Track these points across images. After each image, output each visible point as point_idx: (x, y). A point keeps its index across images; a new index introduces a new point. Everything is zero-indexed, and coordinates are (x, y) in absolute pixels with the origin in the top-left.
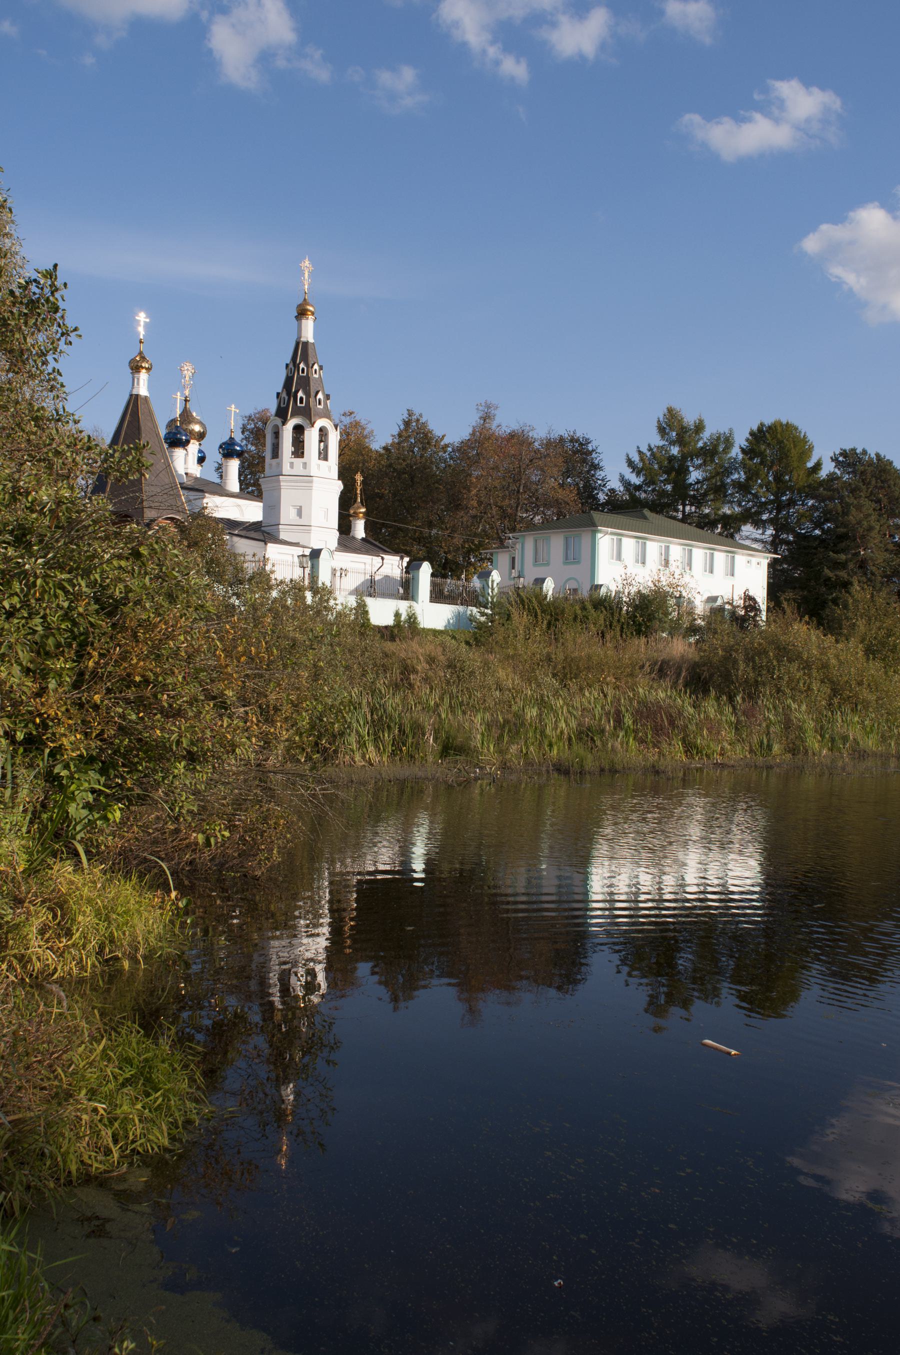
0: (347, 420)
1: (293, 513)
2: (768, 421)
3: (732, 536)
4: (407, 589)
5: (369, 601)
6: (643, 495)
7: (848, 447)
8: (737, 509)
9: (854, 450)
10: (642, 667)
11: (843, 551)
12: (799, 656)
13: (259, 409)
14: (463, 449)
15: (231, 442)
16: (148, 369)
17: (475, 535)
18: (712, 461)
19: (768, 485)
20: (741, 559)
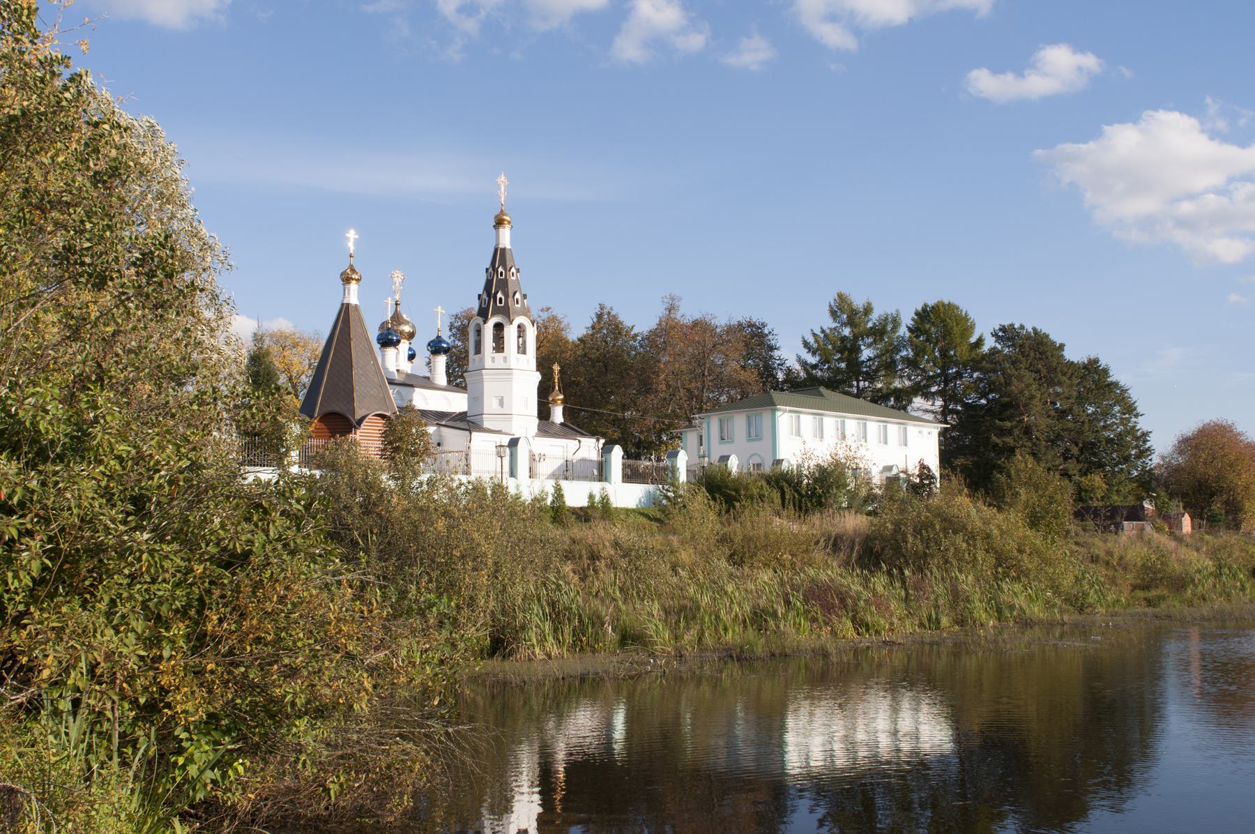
0: (545, 315)
1: (495, 403)
2: (931, 302)
3: (904, 408)
4: (602, 473)
5: (564, 484)
6: (820, 373)
7: (1006, 323)
8: (907, 383)
9: (1012, 325)
10: (817, 543)
11: (1009, 418)
12: (964, 527)
13: (465, 308)
14: (654, 334)
15: (439, 340)
16: (358, 280)
17: (666, 416)
18: (882, 340)
19: (934, 360)
20: (913, 429)
